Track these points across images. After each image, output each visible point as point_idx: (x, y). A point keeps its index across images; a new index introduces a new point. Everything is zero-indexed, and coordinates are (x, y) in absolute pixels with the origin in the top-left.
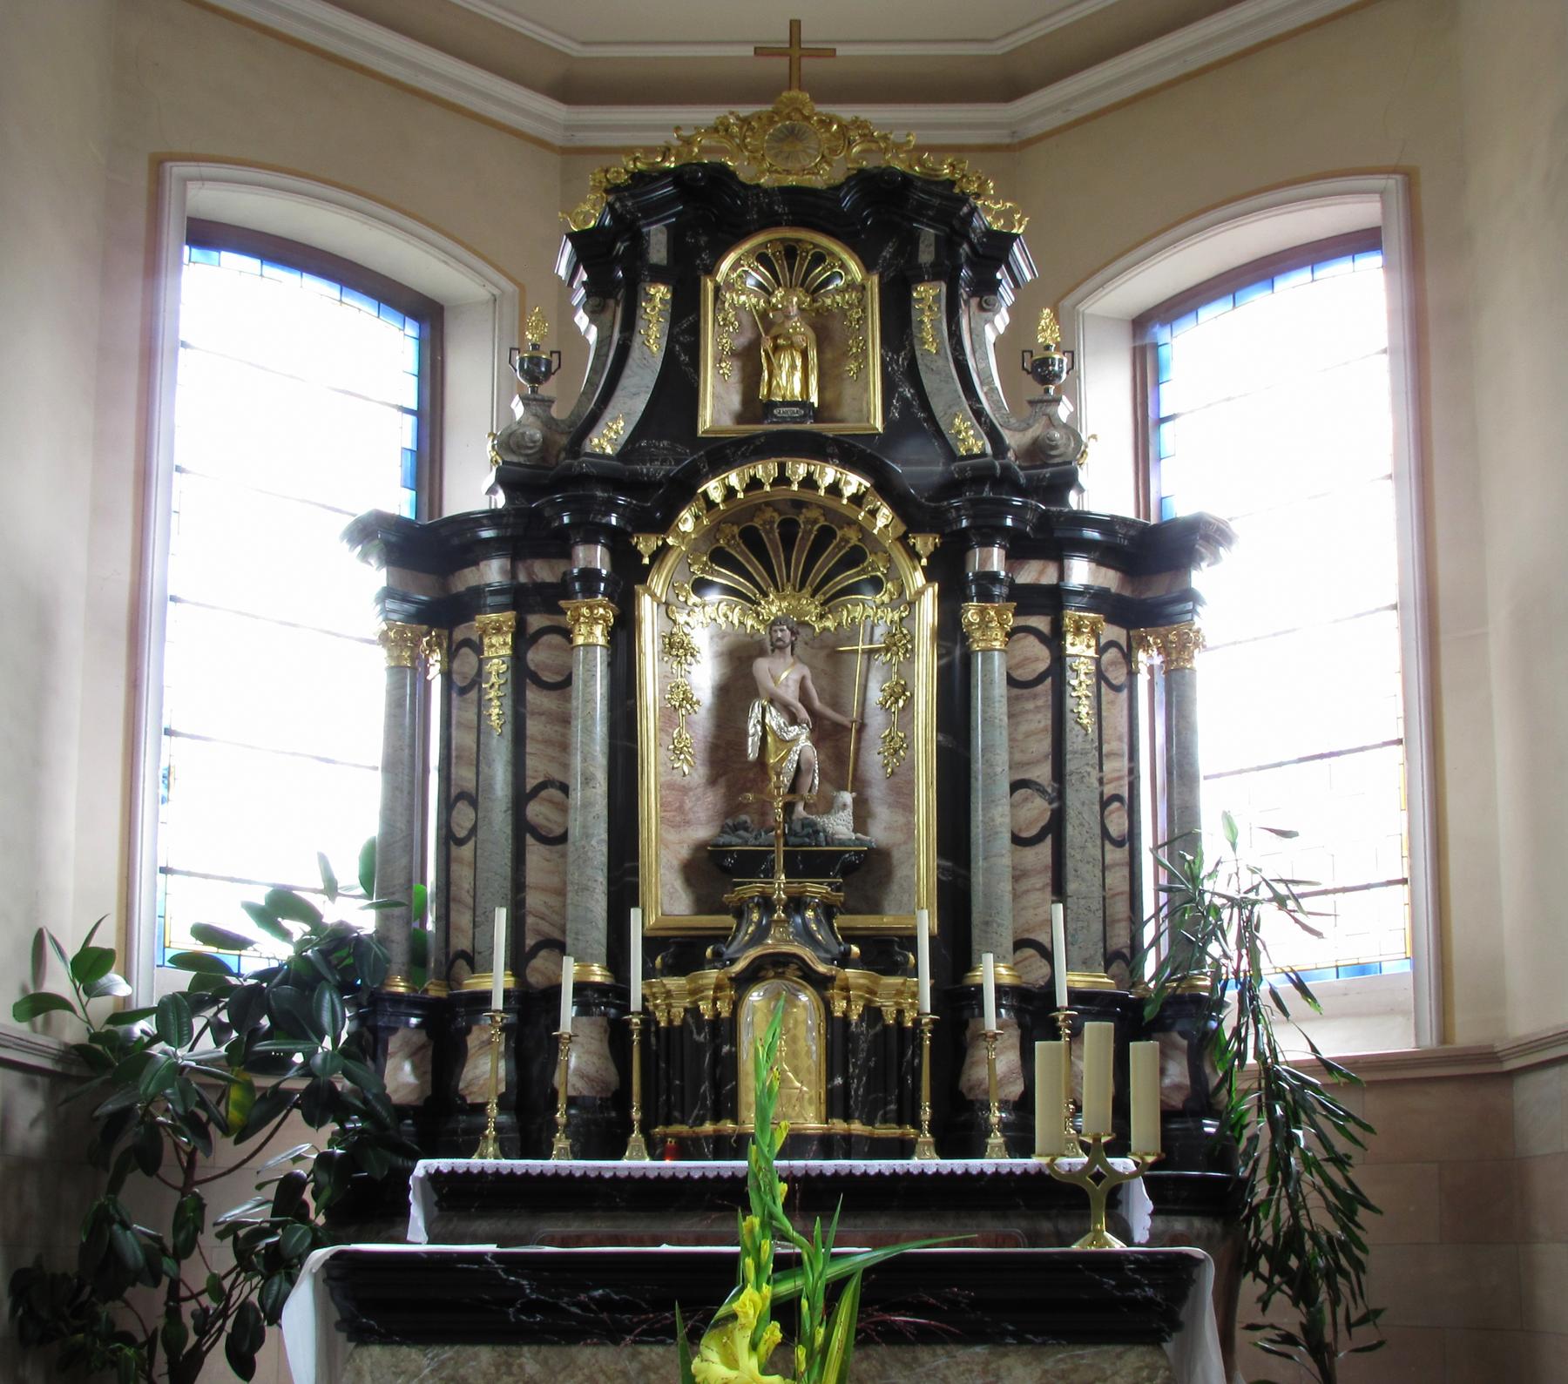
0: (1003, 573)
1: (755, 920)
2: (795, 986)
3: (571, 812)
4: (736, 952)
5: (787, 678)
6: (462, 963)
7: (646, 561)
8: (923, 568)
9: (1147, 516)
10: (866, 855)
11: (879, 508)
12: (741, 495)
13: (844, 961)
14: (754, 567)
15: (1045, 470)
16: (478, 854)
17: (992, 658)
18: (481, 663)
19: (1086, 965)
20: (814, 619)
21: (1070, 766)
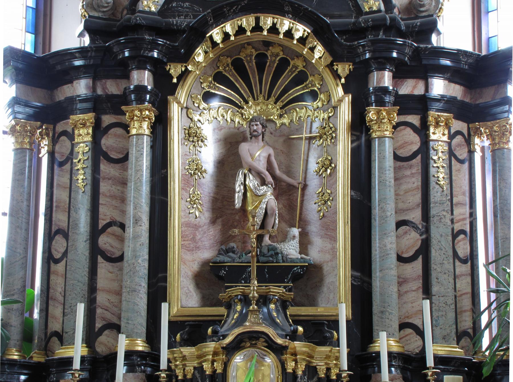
0: (391, 88)
1: (238, 310)
2: (263, 352)
3: (126, 241)
4: (226, 331)
5: (259, 155)
6: (55, 339)
7: (175, 80)
8: (342, 84)
9: (480, 50)
10: (307, 269)
11: (316, 46)
12: (232, 38)
13: (293, 336)
14: (240, 85)
15: (416, 21)
16: (68, 268)
17: (384, 142)
18: (73, 146)
19: (445, 339)
20: (276, 117)
21: (433, 211)
